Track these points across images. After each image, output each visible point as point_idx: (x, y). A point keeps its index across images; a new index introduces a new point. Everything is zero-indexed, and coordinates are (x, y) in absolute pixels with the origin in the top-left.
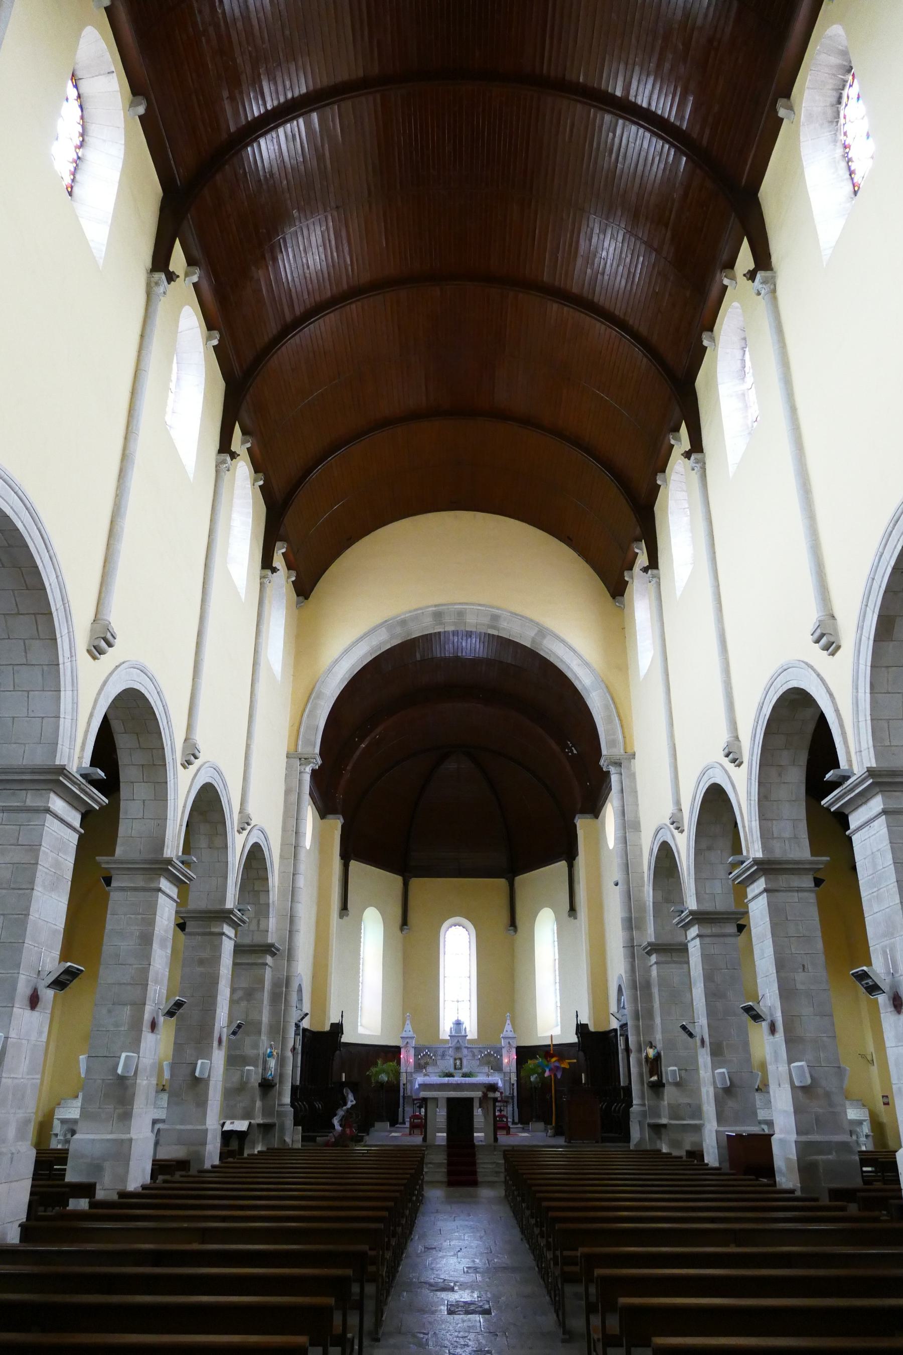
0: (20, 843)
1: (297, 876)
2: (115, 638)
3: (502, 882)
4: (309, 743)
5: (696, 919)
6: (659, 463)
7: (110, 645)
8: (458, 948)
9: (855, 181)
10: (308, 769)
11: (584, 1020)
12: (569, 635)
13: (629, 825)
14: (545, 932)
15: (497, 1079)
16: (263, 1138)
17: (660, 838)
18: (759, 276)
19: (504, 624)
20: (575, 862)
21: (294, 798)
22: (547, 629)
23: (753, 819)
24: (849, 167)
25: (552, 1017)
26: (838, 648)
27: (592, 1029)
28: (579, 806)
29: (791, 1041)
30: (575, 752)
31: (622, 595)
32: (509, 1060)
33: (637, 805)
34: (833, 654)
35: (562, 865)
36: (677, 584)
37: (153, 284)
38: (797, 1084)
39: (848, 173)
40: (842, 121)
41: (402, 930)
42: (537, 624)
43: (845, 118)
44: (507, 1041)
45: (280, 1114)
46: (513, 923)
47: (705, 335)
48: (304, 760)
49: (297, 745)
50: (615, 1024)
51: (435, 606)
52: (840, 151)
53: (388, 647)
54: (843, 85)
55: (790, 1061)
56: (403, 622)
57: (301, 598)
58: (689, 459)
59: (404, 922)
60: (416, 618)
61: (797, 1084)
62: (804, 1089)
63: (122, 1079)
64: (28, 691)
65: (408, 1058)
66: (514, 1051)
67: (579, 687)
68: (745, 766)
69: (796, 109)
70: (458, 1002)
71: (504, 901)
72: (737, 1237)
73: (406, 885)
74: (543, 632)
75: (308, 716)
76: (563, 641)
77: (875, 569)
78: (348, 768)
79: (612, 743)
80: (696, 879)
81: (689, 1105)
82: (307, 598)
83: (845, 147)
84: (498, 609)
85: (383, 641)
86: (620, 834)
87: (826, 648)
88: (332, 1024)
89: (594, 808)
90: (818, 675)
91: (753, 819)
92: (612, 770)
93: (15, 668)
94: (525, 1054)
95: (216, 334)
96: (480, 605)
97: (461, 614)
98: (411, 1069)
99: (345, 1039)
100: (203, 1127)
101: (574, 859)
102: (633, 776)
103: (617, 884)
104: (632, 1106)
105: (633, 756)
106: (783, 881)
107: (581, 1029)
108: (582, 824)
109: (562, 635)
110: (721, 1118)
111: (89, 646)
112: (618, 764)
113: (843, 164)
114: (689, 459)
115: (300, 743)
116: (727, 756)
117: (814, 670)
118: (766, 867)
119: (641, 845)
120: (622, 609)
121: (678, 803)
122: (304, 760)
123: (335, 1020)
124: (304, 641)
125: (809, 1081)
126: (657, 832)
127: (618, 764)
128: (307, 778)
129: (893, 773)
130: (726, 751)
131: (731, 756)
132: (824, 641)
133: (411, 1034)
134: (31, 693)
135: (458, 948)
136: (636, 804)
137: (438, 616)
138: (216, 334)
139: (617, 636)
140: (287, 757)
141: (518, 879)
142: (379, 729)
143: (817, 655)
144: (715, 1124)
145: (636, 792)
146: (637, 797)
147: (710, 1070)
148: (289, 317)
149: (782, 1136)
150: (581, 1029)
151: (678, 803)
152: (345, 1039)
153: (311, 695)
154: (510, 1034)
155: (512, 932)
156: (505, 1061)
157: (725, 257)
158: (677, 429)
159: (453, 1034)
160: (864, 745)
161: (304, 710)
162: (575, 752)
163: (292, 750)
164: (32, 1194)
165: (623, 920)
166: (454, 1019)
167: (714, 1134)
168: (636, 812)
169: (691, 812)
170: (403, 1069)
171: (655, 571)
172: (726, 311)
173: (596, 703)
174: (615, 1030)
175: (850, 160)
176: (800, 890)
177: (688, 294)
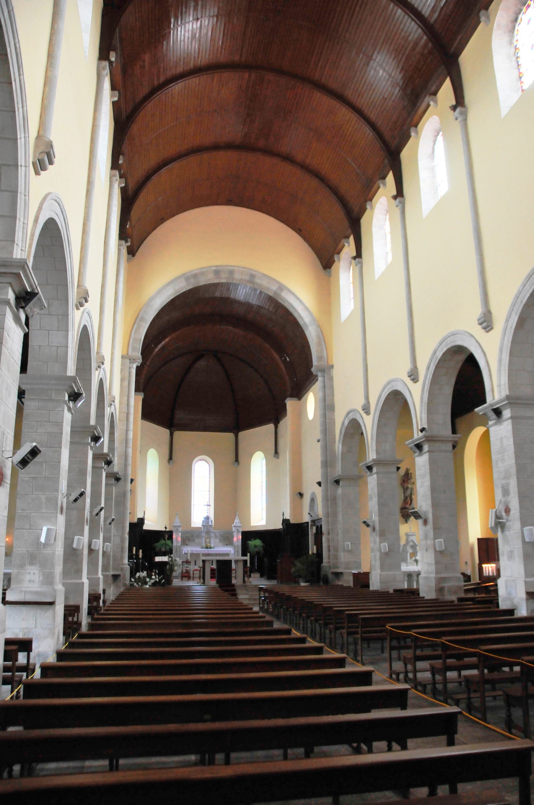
0: (50, 421)
1: (129, 432)
2: (55, 158)
3: (230, 436)
4: (134, 349)
5: (376, 464)
6: (368, 194)
7: (51, 163)
8: (203, 474)
9: (521, 71)
10: (135, 366)
11: (287, 517)
12: (299, 292)
13: (327, 407)
14: (258, 466)
15: (229, 549)
16: (114, 583)
17: (351, 416)
18: (458, 110)
19: (257, 281)
20: (279, 425)
21: (126, 383)
22: (284, 286)
23: (423, 412)
24: (518, 62)
25: (261, 514)
26: (492, 328)
27: (292, 522)
29: (436, 528)
30: (288, 360)
31: (330, 267)
32: (237, 539)
34: (487, 332)
36: (376, 270)
37: (101, 68)
38: (438, 549)
39: (517, 65)
40: (516, 32)
42: (278, 282)
43: (518, 31)
44: (236, 528)
45: (122, 569)
46: (237, 460)
47: (412, 130)
48: (132, 360)
49: (128, 350)
50: (306, 518)
51: (216, 266)
52: (513, 50)
53: (185, 290)
54: (519, 12)
55: (435, 539)
56: (195, 276)
57: (131, 256)
58: (395, 200)
59: (171, 458)
60: (203, 274)
61: (438, 549)
62: (441, 552)
63: (75, 550)
64: (49, 331)
65: (177, 538)
66: (240, 534)
67: (301, 323)
68: (420, 384)
69: (491, 19)
70: (202, 507)
72: (436, 617)
74: (282, 287)
75: (135, 333)
76: (293, 294)
77: (520, 292)
78: (148, 363)
79: (320, 358)
80: (376, 442)
81: (355, 562)
82: (133, 256)
83: (516, 49)
84: (255, 271)
85: (183, 287)
87: (484, 328)
88: (138, 519)
89: (299, 392)
90: (477, 341)
91: (423, 412)
92: (319, 374)
93: (41, 316)
94: (247, 536)
95: (116, 93)
96: (243, 268)
97: (231, 272)
98: (179, 544)
99: (146, 527)
100: (80, 581)
101: (279, 423)
102: (331, 379)
103: (319, 441)
104: (322, 563)
105: (332, 367)
106: (437, 445)
107: (285, 522)
108: (290, 403)
109: (293, 290)
110: (382, 568)
111: (76, 302)
112: (323, 371)
113: (514, 58)
114: (395, 200)
116: (409, 376)
117: (474, 338)
118: (430, 439)
120: (329, 275)
121: (367, 398)
122: (132, 360)
123: (140, 516)
124: (133, 282)
125: (444, 547)
126: (348, 413)
127: (323, 371)
129: (517, 398)
130: (410, 374)
131: (412, 377)
132: (485, 324)
133: (179, 524)
134: (50, 332)
135: (203, 474)
136: (333, 395)
137: (217, 272)
138: (116, 93)
139: (327, 294)
140: (122, 358)
142: (167, 340)
143: (478, 331)
144: (379, 571)
147: (378, 543)
148: (156, 83)
149: (426, 575)
150: (285, 522)
151: (367, 398)
152: (146, 527)
153: (138, 319)
154: (239, 525)
156: (235, 539)
157: (434, 88)
158: (384, 178)
159: (204, 524)
160: (503, 382)
161: (132, 329)
162: (288, 360)
163: (125, 353)
164: (65, 610)
165: (322, 462)
166: (205, 516)
167: (379, 576)
168: (333, 400)
169: (377, 404)
170: (175, 544)
171: (360, 260)
172: (428, 119)
173: (311, 334)
174: (307, 523)
175: (517, 57)
176: (446, 451)
177: (406, 103)
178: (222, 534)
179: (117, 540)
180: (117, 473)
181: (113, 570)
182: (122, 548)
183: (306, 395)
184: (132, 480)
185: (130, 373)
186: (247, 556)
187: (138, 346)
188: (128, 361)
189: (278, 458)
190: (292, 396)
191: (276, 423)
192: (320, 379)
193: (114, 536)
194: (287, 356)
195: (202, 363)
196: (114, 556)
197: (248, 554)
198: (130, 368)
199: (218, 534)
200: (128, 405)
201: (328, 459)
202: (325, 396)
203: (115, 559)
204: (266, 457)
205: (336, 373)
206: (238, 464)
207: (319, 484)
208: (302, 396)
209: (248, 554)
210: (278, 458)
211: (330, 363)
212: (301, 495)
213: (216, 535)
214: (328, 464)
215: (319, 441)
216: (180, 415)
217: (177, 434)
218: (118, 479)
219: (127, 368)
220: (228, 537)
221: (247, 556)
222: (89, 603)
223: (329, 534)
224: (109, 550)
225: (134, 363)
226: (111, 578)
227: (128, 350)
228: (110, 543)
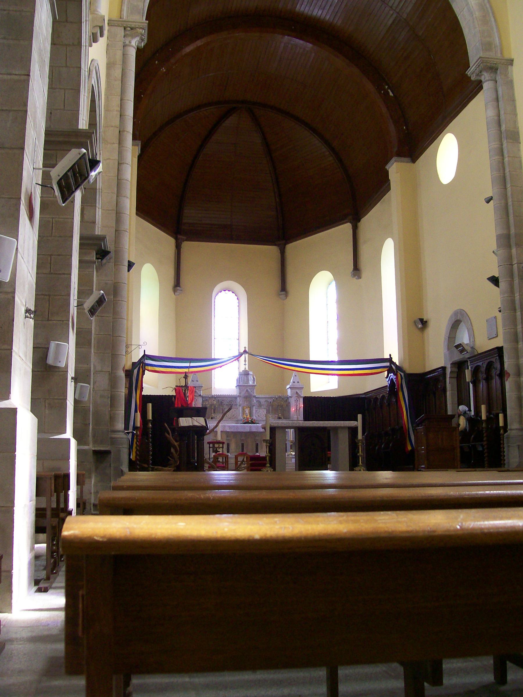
1: (124, 166)
3: (272, 250)
10: (135, 42)
14: (323, 294)
16: (97, 468)
20: (359, 224)
28: (395, 150)
30: (391, 94)
33: (516, 115)
35: (346, 228)
41: (175, 291)
44: (295, 391)
45: (113, 441)
46: (283, 288)
48: (130, 30)
49: (121, 11)
59: (177, 284)
66: (302, 400)
71: (275, 265)
73: (178, 247)
79: (488, 46)
86: (495, 145)
92: (485, 76)
101: (359, 221)
102: (510, 84)
105: (511, 62)
108: (396, 170)
112: (493, 69)
115: (125, 8)
119: (520, 157)
127: (493, 69)
128: (132, 53)
141: (290, 247)
145: (514, 100)
146: (515, 107)
155: (283, 296)
156: (293, 409)
162: (391, 94)
165: (499, 237)
178: (269, 400)
179: (103, 382)
180: (102, 238)
181: (95, 442)
182: (113, 399)
183: (432, 146)
184: (130, 265)
185: (125, 55)
186: (356, 420)
187: (141, 5)
188: (121, 32)
189: (359, 277)
190: (400, 154)
191: (355, 218)
192: (486, 86)
193: (96, 372)
194: (389, 88)
195: (231, 121)
196: (96, 414)
197: (360, 416)
198: (125, 46)
199: (262, 401)
200: (122, 116)
201: (513, 231)
202: (499, 116)
203: (97, 422)
204: (336, 277)
205: (517, 72)
206: (286, 295)
207: (495, 281)
208: (418, 158)
209: (360, 416)
210: (359, 277)
211: (506, 56)
212: (424, 323)
213: (259, 402)
214: (513, 241)
215: (488, 201)
216: (191, 214)
217: (187, 245)
218: (103, 254)
219: (121, 44)
220: (282, 406)
221: (356, 420)
222: (39, 492)
223: (518, 374)
224: (86, 399)
225: (133, 36)
226: (91, 458)
227: (121, 11)
228: (90, 384)
